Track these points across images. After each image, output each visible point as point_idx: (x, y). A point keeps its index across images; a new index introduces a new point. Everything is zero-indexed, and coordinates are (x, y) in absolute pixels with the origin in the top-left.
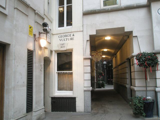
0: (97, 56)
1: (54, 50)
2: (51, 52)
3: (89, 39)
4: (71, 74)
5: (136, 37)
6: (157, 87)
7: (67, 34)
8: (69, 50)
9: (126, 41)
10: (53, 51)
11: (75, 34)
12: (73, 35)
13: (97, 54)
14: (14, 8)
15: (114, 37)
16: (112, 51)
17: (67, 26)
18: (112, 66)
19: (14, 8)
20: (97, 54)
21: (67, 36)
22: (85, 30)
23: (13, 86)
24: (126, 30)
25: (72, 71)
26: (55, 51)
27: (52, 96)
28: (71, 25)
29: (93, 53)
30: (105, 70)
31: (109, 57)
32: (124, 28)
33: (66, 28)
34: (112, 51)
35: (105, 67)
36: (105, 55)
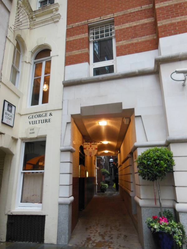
0: (91, 149)
1: (20, 138)
3: (69, 120)
4: (42, 175)
5: (140, 118)
6: (178, 203)
7: (41, 114)
9: (128, 126)
11: (53, 113)
12: (51, 114)
13: (91, 146)
15: (111, 121)
16: (114, 144)
18: (117, 165)
20: (91, 146)
21: (41, 116)
24: (124, 107)
25: (44, 170)
26: (22, 139)
27: (10, 214)
29: (85, 144)
30: (113, 169)
31: (113, 153)
32: (121, 103)
33: (41, 106)
34: (114, 144)
35: (112, 166)
36: (108, 150)
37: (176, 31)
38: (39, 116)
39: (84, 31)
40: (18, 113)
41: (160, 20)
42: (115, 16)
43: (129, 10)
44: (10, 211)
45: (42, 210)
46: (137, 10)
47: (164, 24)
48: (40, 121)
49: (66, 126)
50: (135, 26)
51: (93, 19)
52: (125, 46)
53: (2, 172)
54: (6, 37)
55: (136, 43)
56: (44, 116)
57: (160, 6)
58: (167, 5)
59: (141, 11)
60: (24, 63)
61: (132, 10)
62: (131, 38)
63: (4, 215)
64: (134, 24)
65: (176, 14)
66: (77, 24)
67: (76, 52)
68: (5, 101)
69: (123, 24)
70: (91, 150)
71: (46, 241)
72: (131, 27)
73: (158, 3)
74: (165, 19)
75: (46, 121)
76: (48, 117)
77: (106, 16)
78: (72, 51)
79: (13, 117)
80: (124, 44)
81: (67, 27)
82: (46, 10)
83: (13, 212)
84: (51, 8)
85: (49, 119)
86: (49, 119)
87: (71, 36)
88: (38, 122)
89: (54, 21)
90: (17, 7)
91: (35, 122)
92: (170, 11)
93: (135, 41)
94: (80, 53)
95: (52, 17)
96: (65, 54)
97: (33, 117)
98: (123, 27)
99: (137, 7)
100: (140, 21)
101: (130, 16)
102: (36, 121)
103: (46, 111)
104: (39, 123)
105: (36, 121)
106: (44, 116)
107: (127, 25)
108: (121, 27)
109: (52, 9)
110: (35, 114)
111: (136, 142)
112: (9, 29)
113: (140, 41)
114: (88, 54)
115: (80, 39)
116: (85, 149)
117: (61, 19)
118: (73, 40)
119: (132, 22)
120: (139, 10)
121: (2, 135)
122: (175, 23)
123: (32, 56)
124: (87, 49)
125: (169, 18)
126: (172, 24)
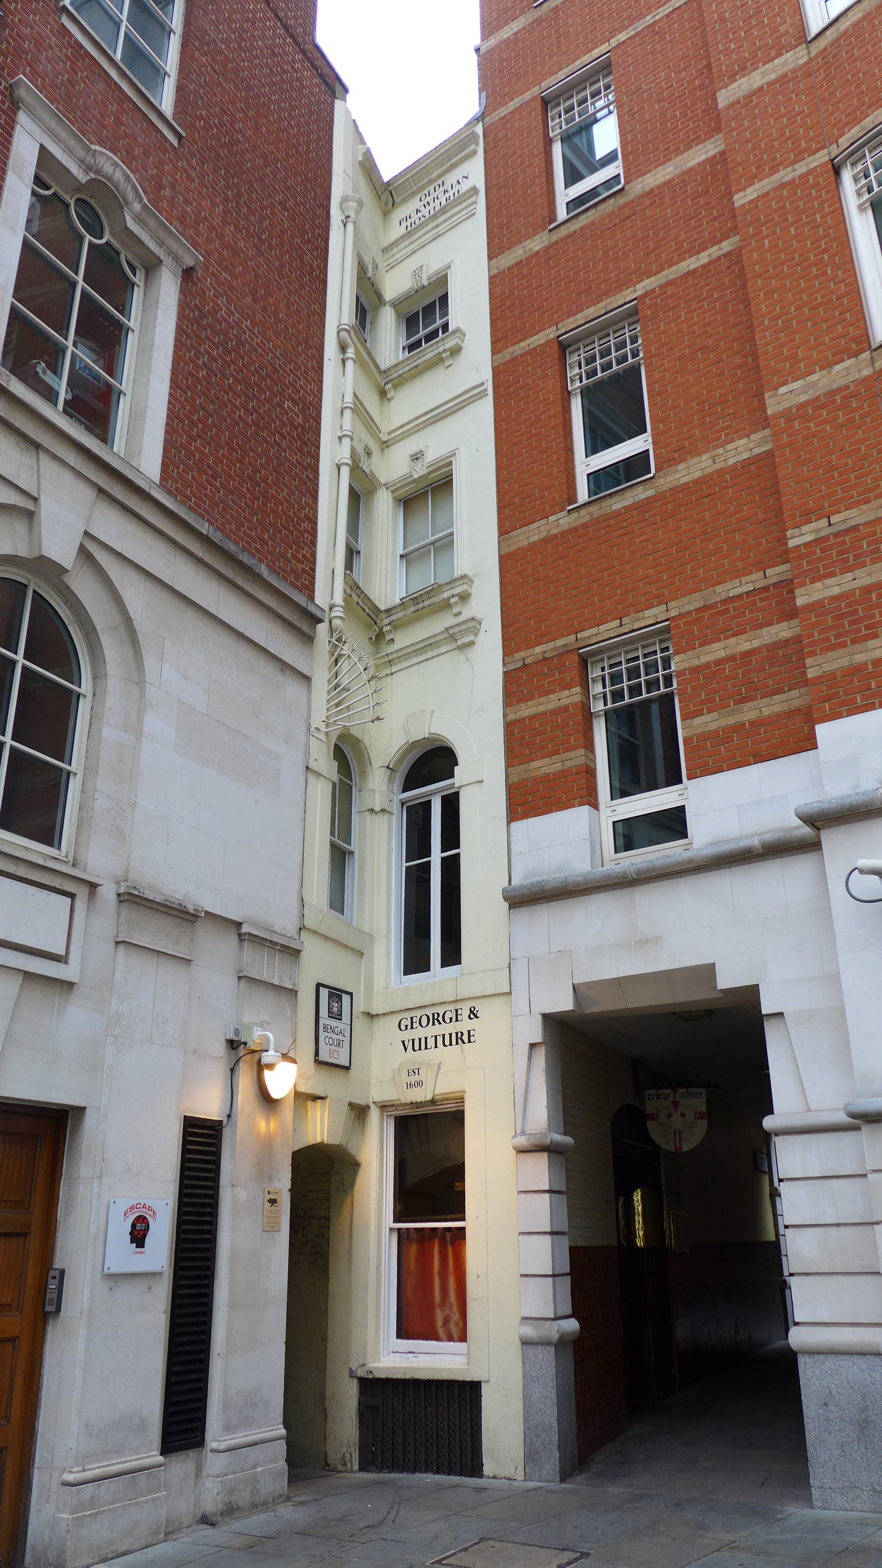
2: (359, 1112)
3: (537, 1036)
8: (446, 1099)
10: (372, 1106)
11: (481, 1008)
12: (473, 1015)
13: (676, 1104)
14: (117, 943)
17: (442, 967)
19: (117, 943)
21: (440, 1019)
22: (520, 988)
23: (86, 1305)
25: (463, 1219)
26: (383, 1107)
28: (457, 961)
32: (711, 968)
37: (870, 697)
38: (435, 1019)
39: (565, 678)
40: (363, 1013)
41: (813, 654)
42: (674, 613)
43: (719, 589)
44: (364, 1365)
45: (468, 1364)
46: (750, 587)
47: (827, 668)
48: (440, 1039)
49: (530, 1058)
50: (746, 654)
51: (594, 630)
52: (715, 734)
53: (328, 1227)
54: (307, 768)
55: (752, 723)
56: (451, 1019)
57: (810, 596)
58: (837, 590)
59: (765, 589)
60: (368, 814)
61: (733, 588)
62: (736, 703)
63: (347, 1375)
64: (742, 644)
65: (867, 627)
66: (538, 649)
67: (543, 766)
68: (319, 985)
69: (702, 645)
70: (677, 1122)
71: (488, 1468)
72: (732, 658)
73: (805, 585)
74: (831, 648)
75: (459, 1038)
76: (465, 1025)
77: (640, 614)
78: (529, 761)
79: (348, 1034)
80: (713, 726)
81: (504, 665)
82: (426, 603)
83: (374, 1368)
84: (446, 595)
85: (469, 1032)
86: (469, 1032)
87: (520, 701)
88: (431, 1042)
89: (459, 643)
90: (330, 642)
91: (421, 1045)
92: (846, 615)
93: (749, 713)
94: (558, 767)
95: (451, 632)
96: (507, 777)
97: (415, 1025)
98: (703, 659)
99: (750, 573)
100: (765, 630)
101: (727, 611)
102: (426, 1038)
103: (456, 1001)
104: (436, 1047)
105: (426, 1038)
106: (451, 1019)
107: (717, 651)
108: (698, 657)
109: (449, 598)
110: (419, 1013)
111: (771, 1111)
112: (312, 740)
113: (766, 712)
114: (590, 773)
115: (554, 712)
116: (652, 1117)
117: (482, 633)
118: (532, 718)
119: (733, 636)
120: (759, 585)
121: (319, 1101)
122: (865, 664)
123: (391, 780)
124: (581, 751)
125: (843, 645)
126: (857, 670)
